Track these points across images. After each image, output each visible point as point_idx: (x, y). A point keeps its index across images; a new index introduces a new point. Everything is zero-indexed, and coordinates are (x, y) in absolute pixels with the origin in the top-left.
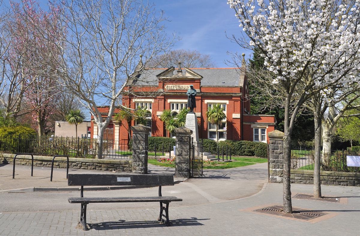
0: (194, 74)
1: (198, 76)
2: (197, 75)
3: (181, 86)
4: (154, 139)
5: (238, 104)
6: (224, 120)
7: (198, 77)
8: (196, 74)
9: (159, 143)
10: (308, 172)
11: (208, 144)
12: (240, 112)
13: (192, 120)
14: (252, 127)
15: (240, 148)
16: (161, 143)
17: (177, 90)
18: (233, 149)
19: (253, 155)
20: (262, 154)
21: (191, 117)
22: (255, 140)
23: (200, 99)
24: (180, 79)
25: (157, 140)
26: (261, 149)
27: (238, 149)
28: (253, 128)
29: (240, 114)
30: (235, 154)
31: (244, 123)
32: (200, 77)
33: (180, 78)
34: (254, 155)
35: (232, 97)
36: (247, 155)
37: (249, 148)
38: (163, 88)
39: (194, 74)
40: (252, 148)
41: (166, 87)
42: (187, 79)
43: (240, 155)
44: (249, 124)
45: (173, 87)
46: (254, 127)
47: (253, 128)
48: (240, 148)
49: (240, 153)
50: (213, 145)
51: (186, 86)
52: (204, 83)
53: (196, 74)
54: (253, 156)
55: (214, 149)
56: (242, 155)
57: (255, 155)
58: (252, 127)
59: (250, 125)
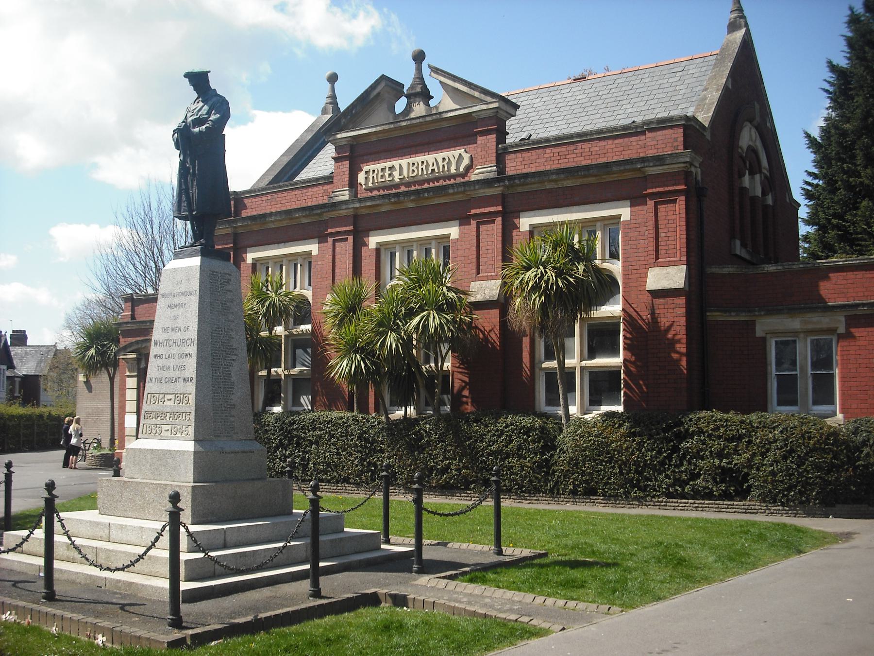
0: (471, 92)
1: (489, 99)
2: (482, 96)
3: (419, 159)
4: (291, 424)
5: (675, 215)
6: (613, 309)
7: (484, 107)
8: (477, 94)
9: (311, 443)
10: (64, 609)
11: (511, 441)
12: (684, 258)
14: (759, 333)
15: (669, 457)
16: (317, 443)
17: (403, 182)
18: (637, 464)
19: (743, 494)
20: (790, 489)
21: (179, 283)
22: (780, 403)
23: (496, 213)
24: (418, 130)
25: (302, 428)
26: (785, 458)
27: (662, 463)
28: (764, 340)
29: (685, 267)
30: (644, 489)
31: (715, 316)
32: (496, 105)
33: (414, 122)
34: (748, 491)
35: (648, 180)
36: (709, 496)
37: (720, 455)
38: (353, 183)
39: (471, 92)
40: (736, 452)
41: (361, 178)
42: (445, 124)
43: (670, 495)
44: (743, 318)
45: (387, 173)
46: (774, 333)
47: (764, 340)
48: (669, 457)
49: (669, 486)
50: (534, 442)
51: (440, 156)
52: (516, 130)
53: (477, 94)
54: (745, 499)
55: (540, 467)
56: (683, 496)
57: (755, 493)
58: (759, 333)
59: (751, 325)
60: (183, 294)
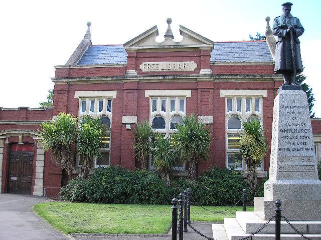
13: (300, 110)
60: (298, 107)
